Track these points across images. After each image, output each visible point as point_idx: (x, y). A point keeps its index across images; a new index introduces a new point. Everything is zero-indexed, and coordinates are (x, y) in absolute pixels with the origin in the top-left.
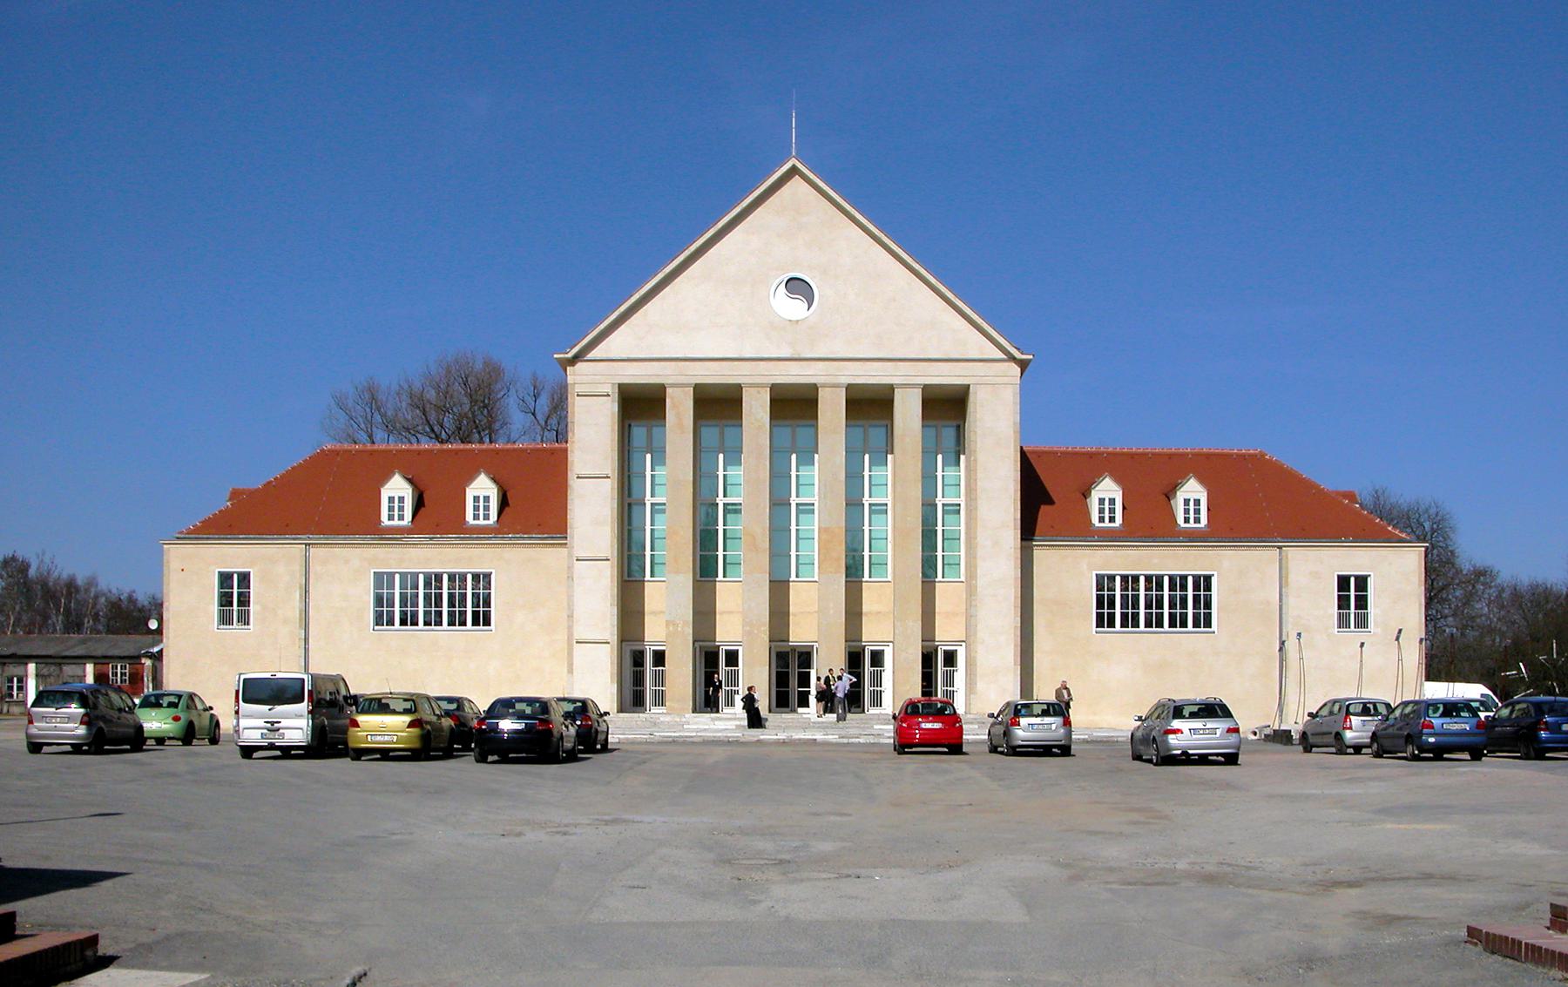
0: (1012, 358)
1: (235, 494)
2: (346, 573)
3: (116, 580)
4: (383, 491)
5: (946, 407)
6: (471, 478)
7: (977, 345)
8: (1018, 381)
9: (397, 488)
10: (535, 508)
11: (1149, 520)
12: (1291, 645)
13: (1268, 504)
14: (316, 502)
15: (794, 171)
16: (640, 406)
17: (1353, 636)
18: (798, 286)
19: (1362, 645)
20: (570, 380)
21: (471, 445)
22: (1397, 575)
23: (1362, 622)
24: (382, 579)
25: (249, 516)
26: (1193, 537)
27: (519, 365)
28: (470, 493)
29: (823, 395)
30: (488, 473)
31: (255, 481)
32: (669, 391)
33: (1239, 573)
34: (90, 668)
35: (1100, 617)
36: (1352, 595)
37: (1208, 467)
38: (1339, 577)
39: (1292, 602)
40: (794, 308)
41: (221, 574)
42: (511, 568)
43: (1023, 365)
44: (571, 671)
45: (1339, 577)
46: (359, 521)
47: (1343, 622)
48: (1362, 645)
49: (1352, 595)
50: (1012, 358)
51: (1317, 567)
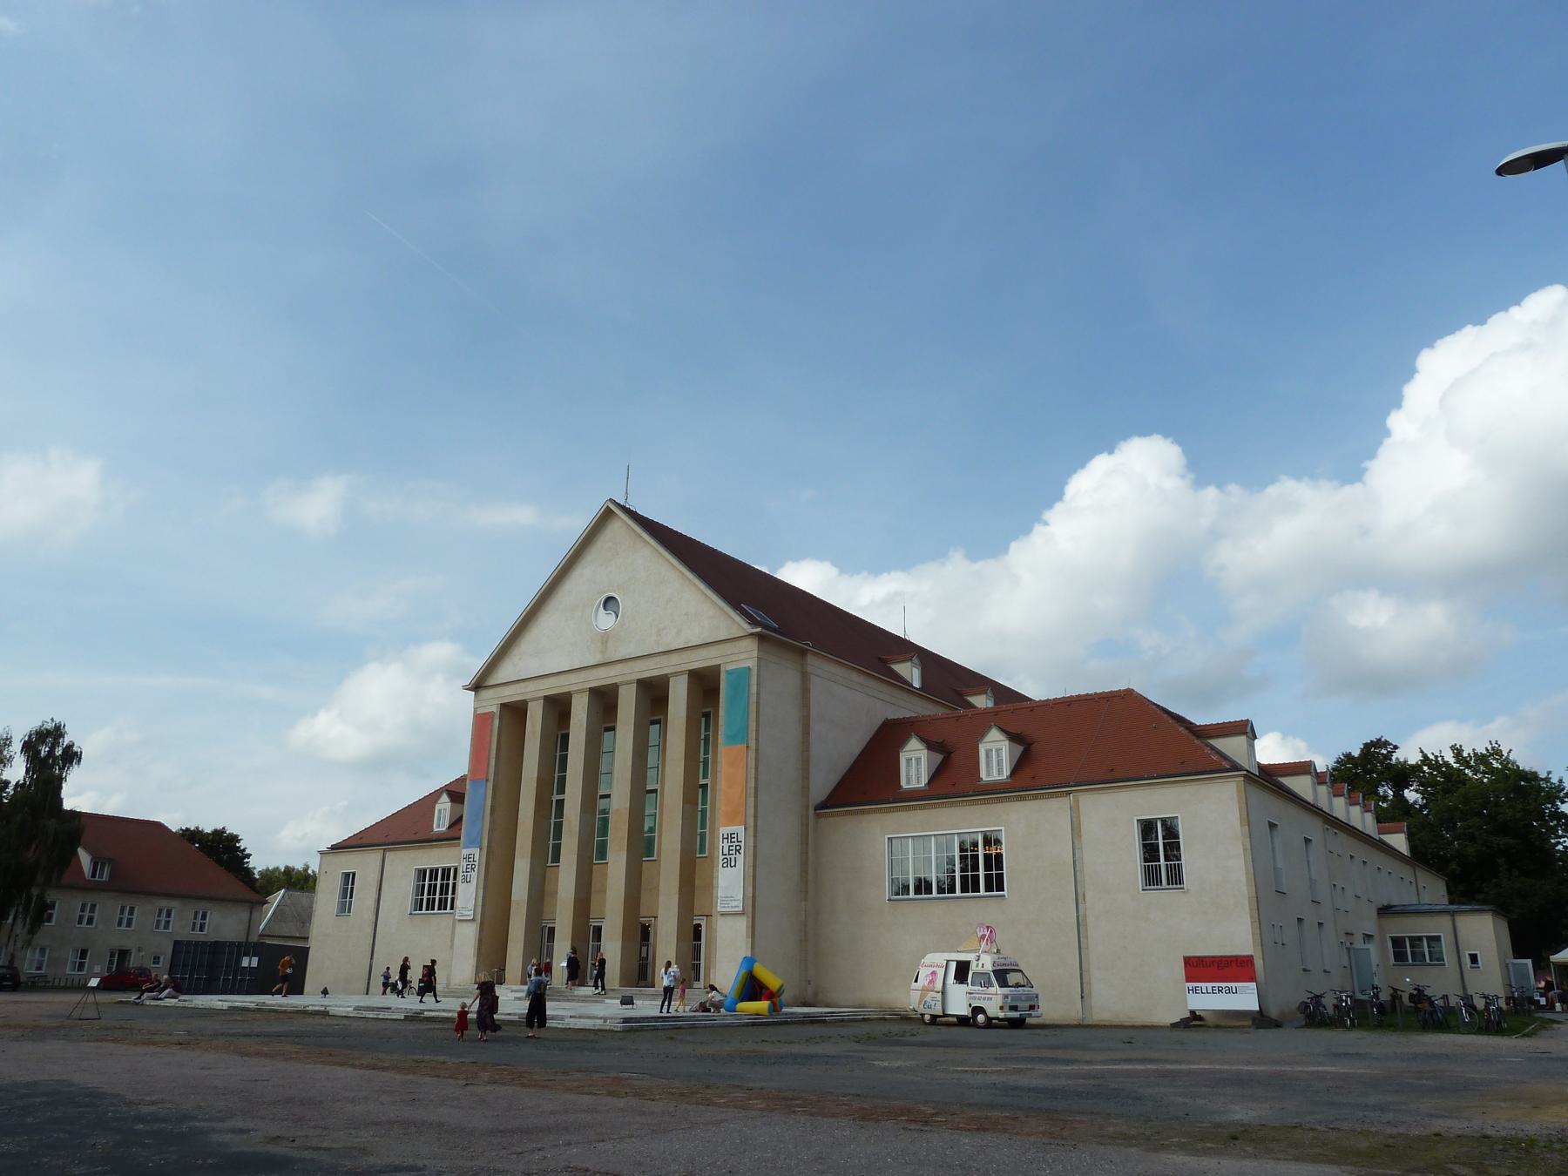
18: (609, 602)
22: (1210, 816)
23: (1176, 877)
33: (1029, 830)
36: (1160, 850)
40: (606, 621)
47: (1152, 878)
49: (1160, 850)
51: (1113, 817)
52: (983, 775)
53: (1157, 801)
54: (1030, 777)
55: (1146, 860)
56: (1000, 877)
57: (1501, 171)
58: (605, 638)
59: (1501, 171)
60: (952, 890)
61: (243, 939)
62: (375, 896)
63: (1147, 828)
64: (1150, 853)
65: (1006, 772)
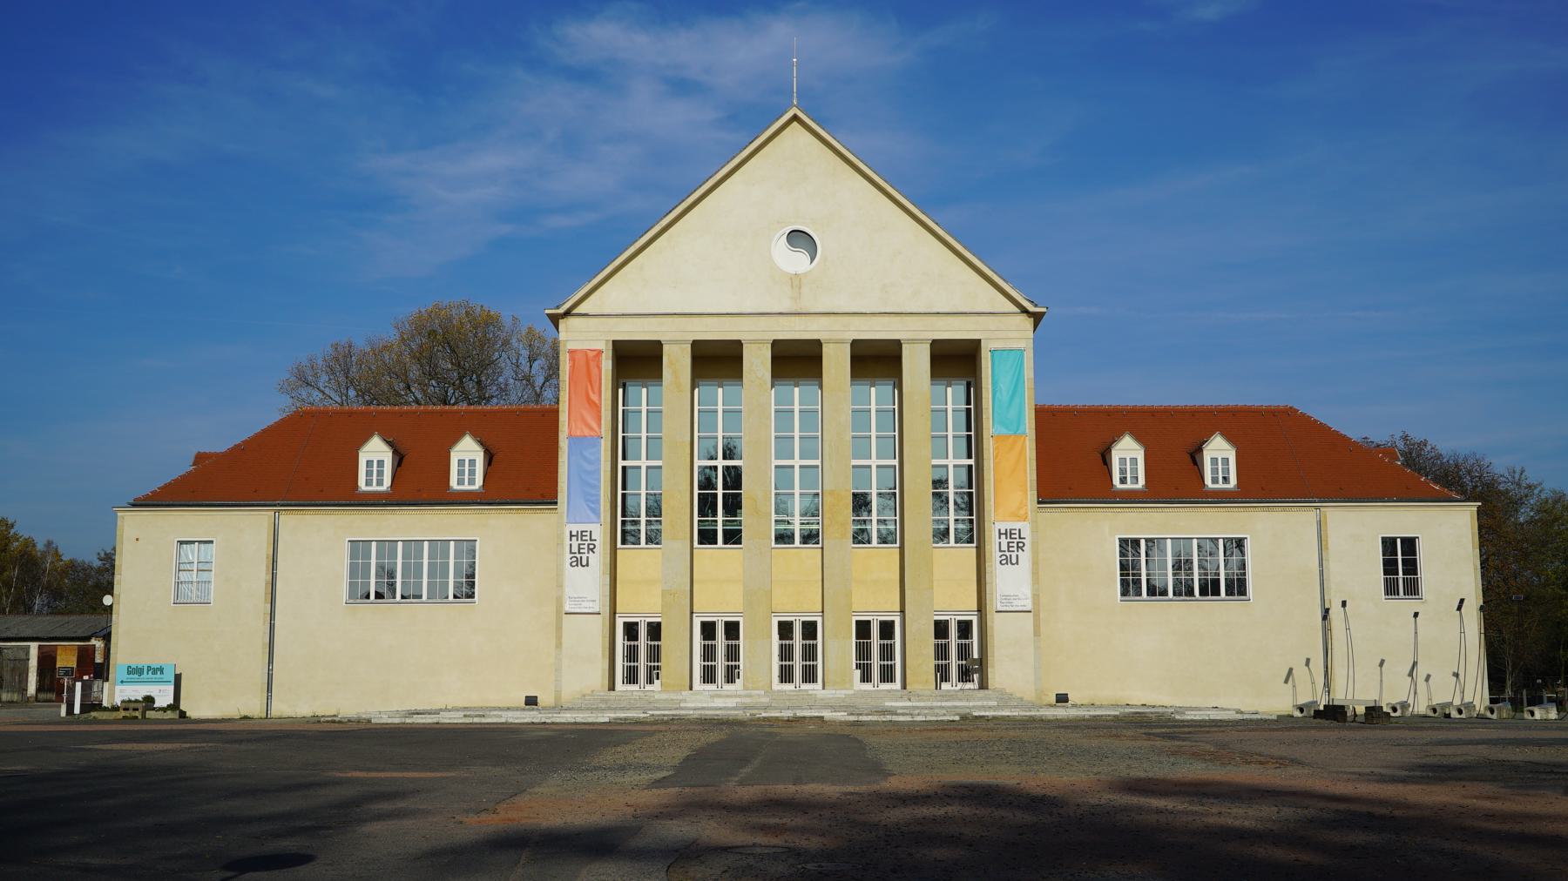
0: (1025, 311)
1: (200, 458)
2: (319, 540)
3: (78, 549)
4: (1113, 452)
5: (957, 360)
6: (456, 439)
7: (989, 298)
8: (1031, 334)
9: (376, 454)
10: (523, 477)
11: (1175, 479)
12: (1336, 612)
13: (1298, 461)
14: (286, 468)
15: (795, 118)
16: (637, 361)
17: (1405, 605)
18: (799, 238)
19: (1416, 615)
20: (562, 336)
21: (455, 408)
22: (1449, 537)
23: (1412, 589)
24: (358, 548)
25: (214, 483)
26: (1130, 498)
27: (517, 313)
28: (455, 457)
29: (827, 351)
30: (475, 436)
31: (221, 446)
32: (665, 348)
33: (1277, 536)
34: (34, 647)
35: (1124, 584)
36: (1400, 563)
37: (1231, 422)
38: (1384, 540)
39: (1334, 567)
40: (797, 261)
41: (1123, 542)
42: (502, 537)
43: (1037, 318)
44: (559, 645)
45: (1384, 540)
46: (333, 488)
47: (1391, 589)
48: (1416, 615)
49: (1400, 563)
50: (1025, 311)
51: (1360, 529)
52: (454, 483)
53: (1400, 519)
54: (1259, 486)
55: (1386, 573)
56: (353, 555)
57: (1462, 601)
58: (796, 281)
59: (1462, 601)
60: (1216, 592)
61: (1310, 692)
62: (263, 576)
63: (1389, 544)
64: (1389, 567)
65: (479, 483)
